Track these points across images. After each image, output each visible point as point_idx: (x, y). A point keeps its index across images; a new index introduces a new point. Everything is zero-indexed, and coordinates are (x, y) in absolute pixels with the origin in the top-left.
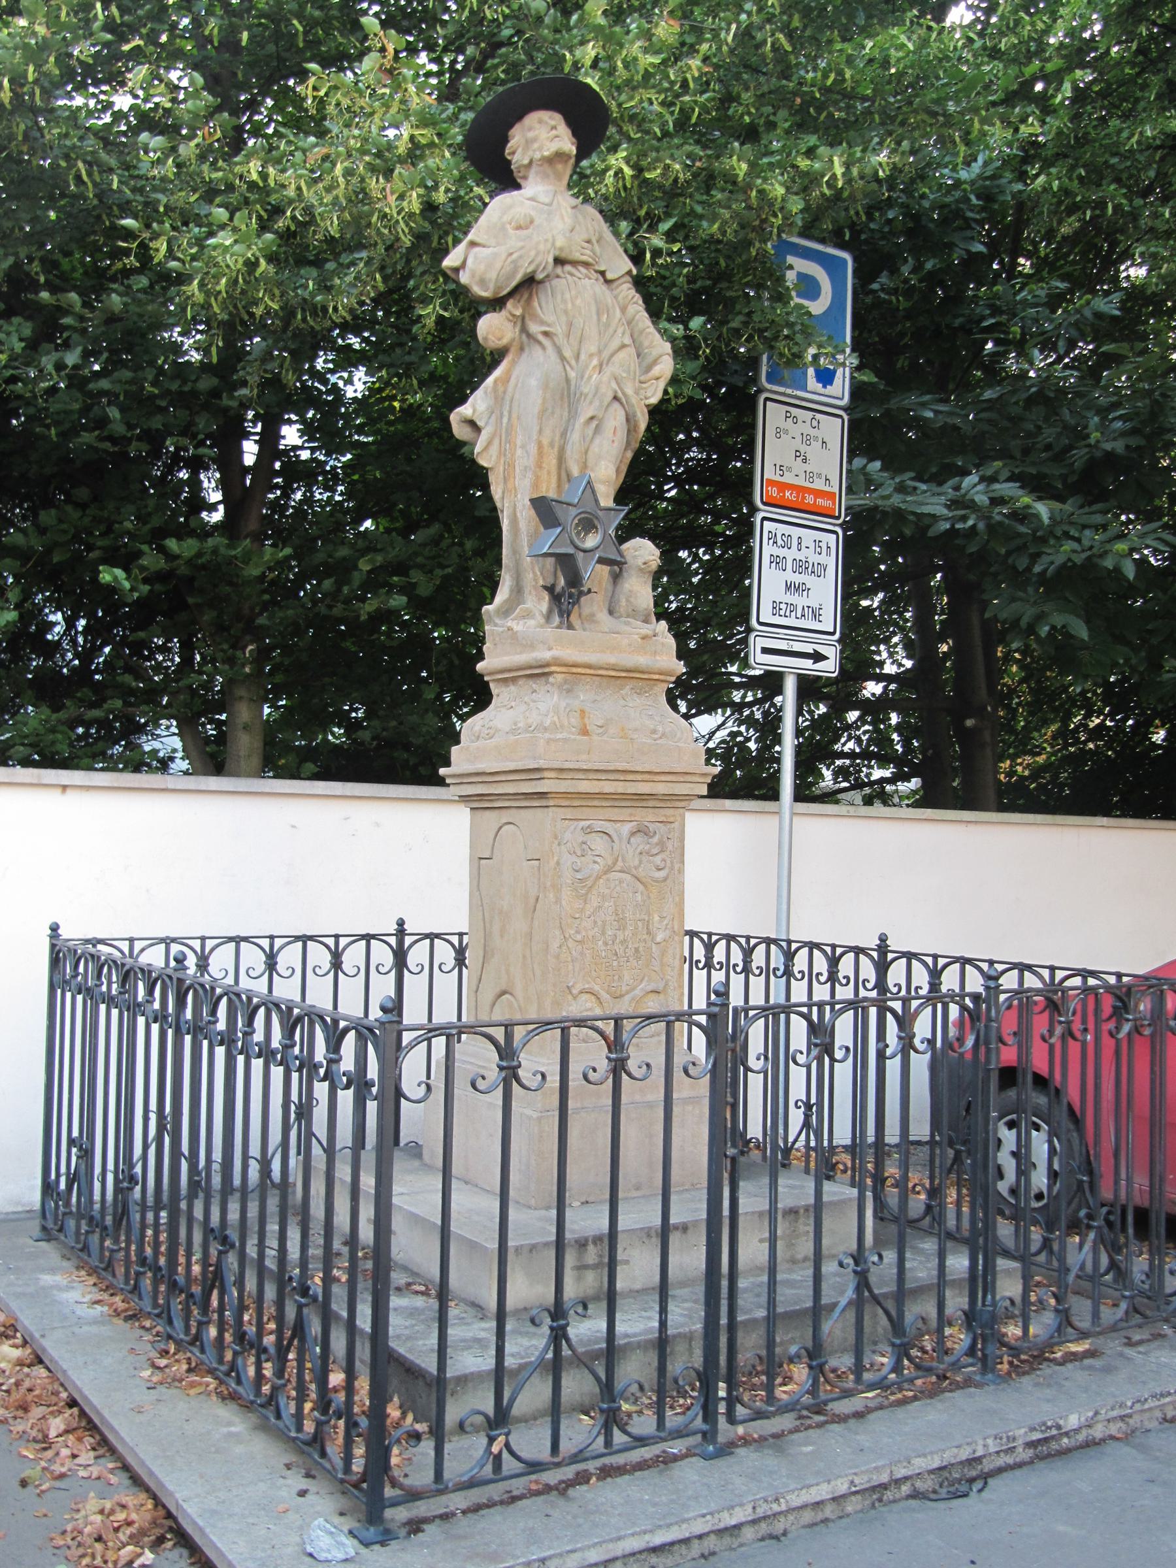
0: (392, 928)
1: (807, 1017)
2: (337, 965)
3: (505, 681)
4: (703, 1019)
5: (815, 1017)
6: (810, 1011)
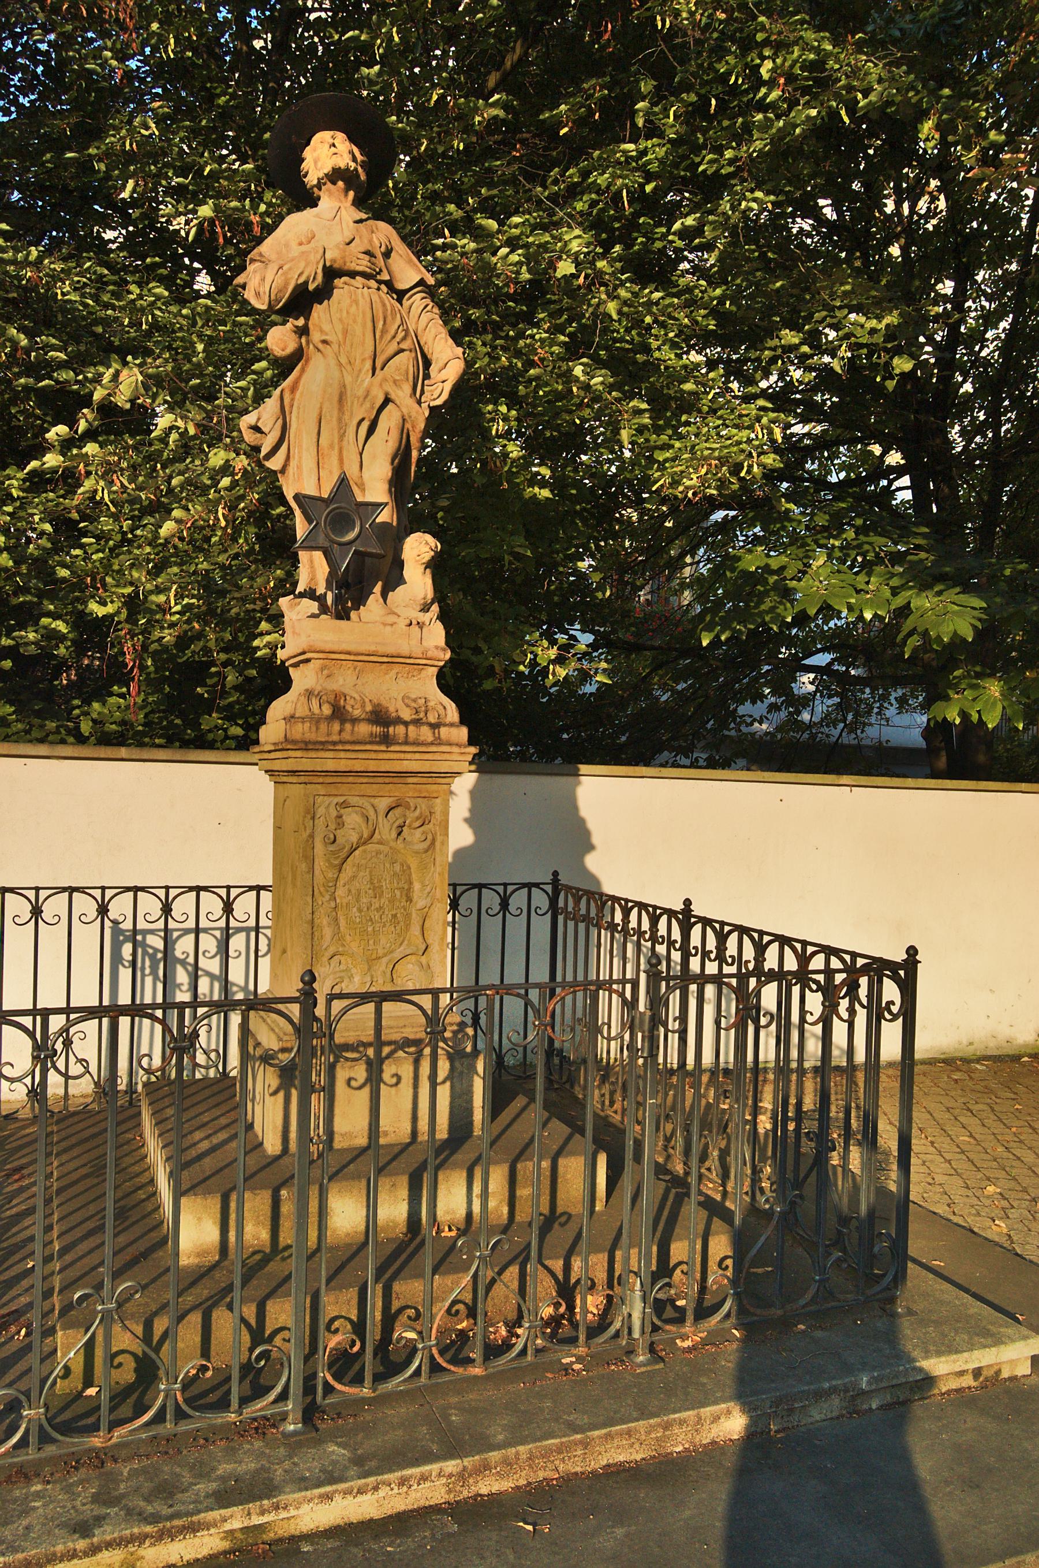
0: (549, 878)
1: (622, 995)
2: (504, 905)
3: (296, 665)
4: (734, 981)
5: (628, 995)
6: (624, 988)
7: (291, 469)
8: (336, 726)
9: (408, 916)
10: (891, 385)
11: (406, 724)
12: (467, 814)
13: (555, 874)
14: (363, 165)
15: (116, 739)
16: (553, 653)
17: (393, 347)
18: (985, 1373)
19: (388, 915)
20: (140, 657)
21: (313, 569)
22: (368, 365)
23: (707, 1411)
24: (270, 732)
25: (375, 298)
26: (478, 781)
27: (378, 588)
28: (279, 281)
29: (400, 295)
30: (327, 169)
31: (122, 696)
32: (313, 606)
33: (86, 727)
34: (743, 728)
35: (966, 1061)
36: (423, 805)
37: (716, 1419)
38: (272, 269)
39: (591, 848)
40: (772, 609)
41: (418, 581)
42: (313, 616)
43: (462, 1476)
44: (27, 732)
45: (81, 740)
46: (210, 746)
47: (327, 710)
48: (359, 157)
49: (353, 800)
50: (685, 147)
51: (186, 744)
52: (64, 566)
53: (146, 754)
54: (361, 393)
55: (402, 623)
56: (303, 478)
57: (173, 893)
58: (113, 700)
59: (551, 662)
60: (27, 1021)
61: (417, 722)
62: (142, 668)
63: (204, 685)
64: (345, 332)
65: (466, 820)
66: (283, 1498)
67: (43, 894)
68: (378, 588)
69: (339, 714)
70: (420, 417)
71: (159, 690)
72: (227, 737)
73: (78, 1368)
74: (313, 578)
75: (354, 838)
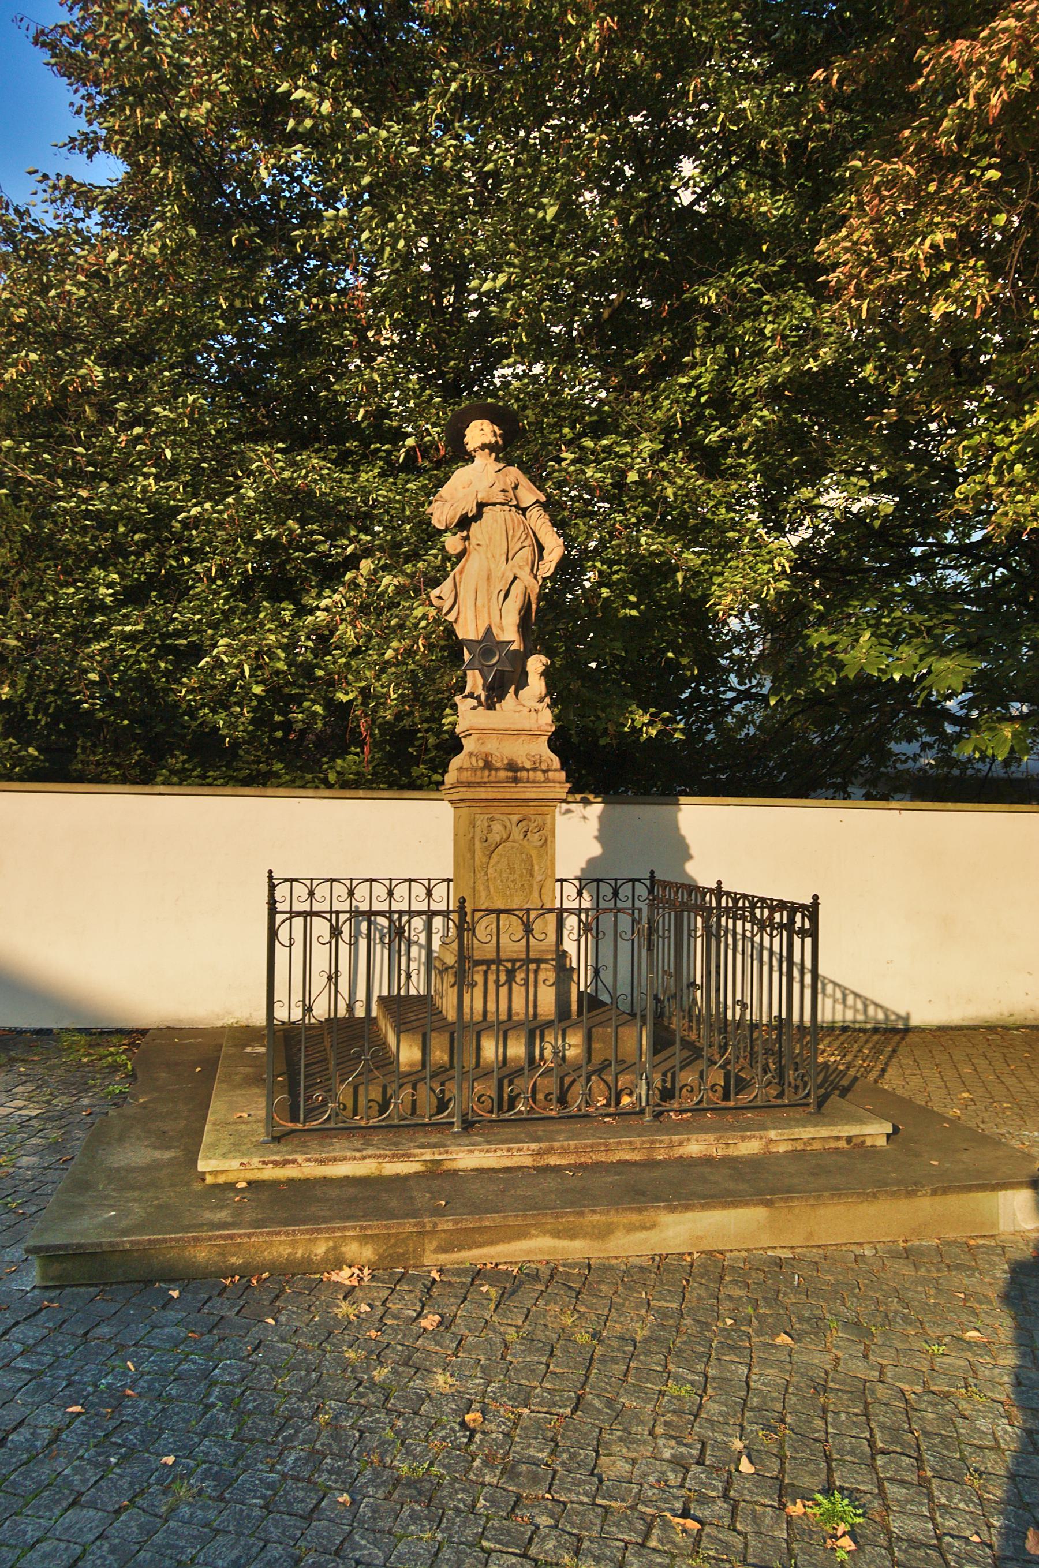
0: (648, 876)
7: (460, 620)
8: (486, 773)
9: (531, 886)
10: (877, 523)
11: (528, 770)
12: (596, 833)
13: (652, 872)
14: (501, 435)
15: (353, 784)
16: (646, 719)
17: (519, 545)
18: (854, 1141)
19: (519, 884)
20: (370, 728)
21: (475, 681)
22: (504, 558)
23: (676, 1138)
24: (450, 778)
25: (508, 517)
26: (604, 811)
27: (512, 689)
28: (451, 513)
29: (524, 511)
30: (479, 444)
31: (357, 754)
32: (475, 703)
33: (332, 777)
34: (899, 765)
35: (1006, 1028)
36: (539, 819)
37: (681, 1144)
38: (448, 505)
39: (690, 857)
40: (822, 677)
41: (536, 685)
42: (474, 708)
43: (540, 1153)
44: (293, 782)
45: (330, 786)
46: (420, 788)
47: (481, 764)
48: (498, 432)
49: (497, 816)
50: (721, 381)
51: (402, 787)
52: (321, 668)
53: (375, 794)
54: (500, 574)
55: (526, 710)
56: (468, 630)
57: (394, 883)
58: (350, 757)
59: (644, 724)
60: (328, 916)
61: (535, 769)
62: (372, 735)
63: (413, 746)
64: (490, 539)
65: (596, 838)
66: (450, 1149)
67: (315, 883)
68: (512, 689)
69: (488, 765)
70: (535, 589)
71: (382, 750)
72: (430, 782)
73: (350, 1104)
74: (475, 685)
75: (498, 839)
